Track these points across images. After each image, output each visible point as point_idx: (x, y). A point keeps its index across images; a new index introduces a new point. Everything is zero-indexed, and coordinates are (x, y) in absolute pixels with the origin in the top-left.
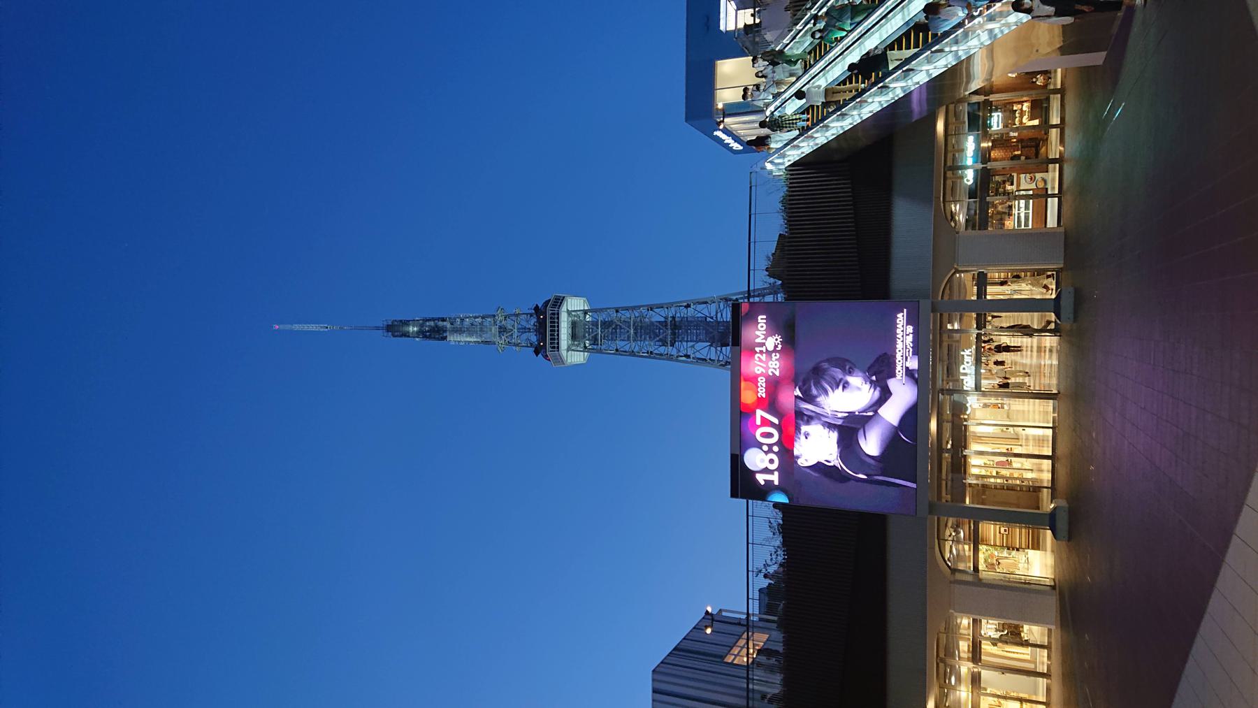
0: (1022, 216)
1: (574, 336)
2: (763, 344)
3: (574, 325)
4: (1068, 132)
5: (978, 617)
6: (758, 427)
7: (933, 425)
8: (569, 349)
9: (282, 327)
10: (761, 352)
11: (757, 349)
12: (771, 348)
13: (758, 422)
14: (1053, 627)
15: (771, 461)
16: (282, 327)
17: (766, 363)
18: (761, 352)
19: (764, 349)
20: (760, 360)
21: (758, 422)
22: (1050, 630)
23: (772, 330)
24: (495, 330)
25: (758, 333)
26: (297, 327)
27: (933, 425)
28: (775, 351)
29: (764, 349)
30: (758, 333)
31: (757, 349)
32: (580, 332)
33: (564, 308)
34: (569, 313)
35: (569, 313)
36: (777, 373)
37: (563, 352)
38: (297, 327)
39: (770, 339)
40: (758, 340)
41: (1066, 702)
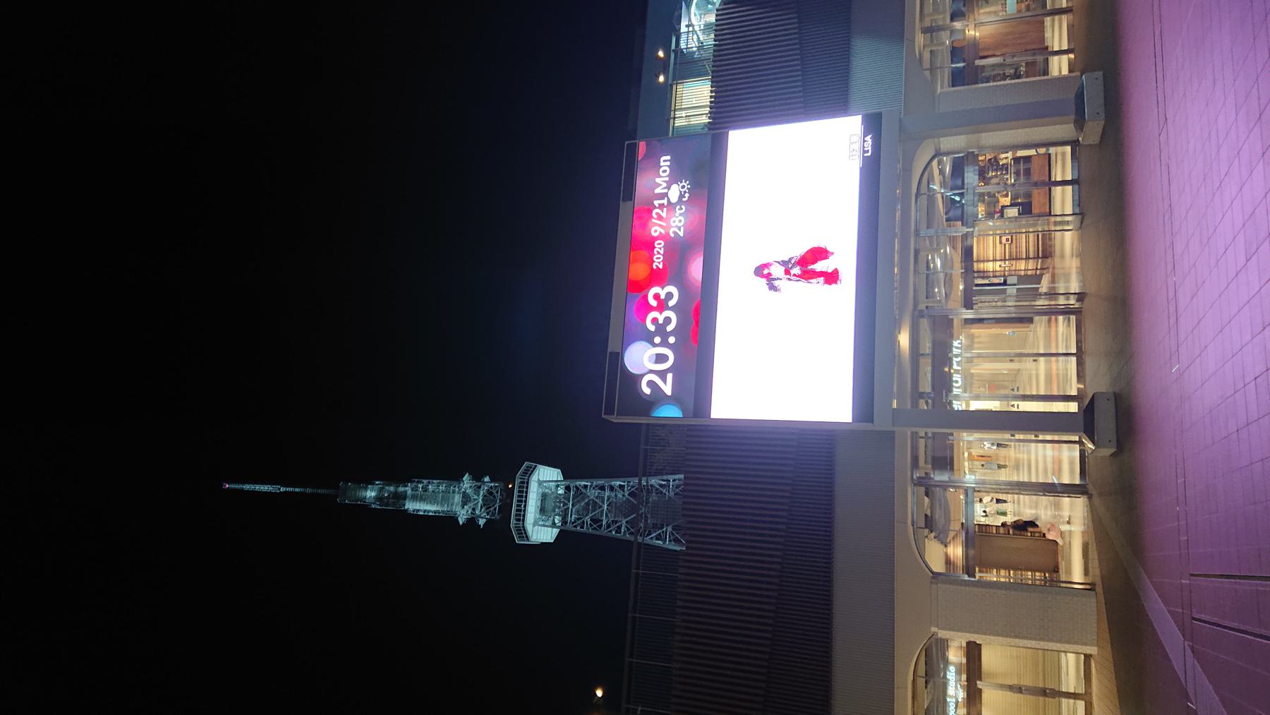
0: (1040, 459)
1: (542, 510)
2: (666, 195)
3: (544, 497)
4: (1089, 363)
6: (652, 309)
8: (535, 523)
9: (233, 486)
11: (656, 203)
12: (674, 199)
13: (670, 376)
15: (661, 358)
16: (233, 486)
17: (667, 220)
19: (665, 202)
20: (660, 217)
21: (670, 376)
24: (458, 498)
25: (658, 180)
26: (247, 487)
29: (665, 202)
30: (658, 180)
31: (656, 203)
32: (550, 504)
33: (534, 478)
34: (540, 483)
35: (540, 483)
36: (681, 234)
38: (247, 487)
40: (658, 191)
41: (1119, 713)
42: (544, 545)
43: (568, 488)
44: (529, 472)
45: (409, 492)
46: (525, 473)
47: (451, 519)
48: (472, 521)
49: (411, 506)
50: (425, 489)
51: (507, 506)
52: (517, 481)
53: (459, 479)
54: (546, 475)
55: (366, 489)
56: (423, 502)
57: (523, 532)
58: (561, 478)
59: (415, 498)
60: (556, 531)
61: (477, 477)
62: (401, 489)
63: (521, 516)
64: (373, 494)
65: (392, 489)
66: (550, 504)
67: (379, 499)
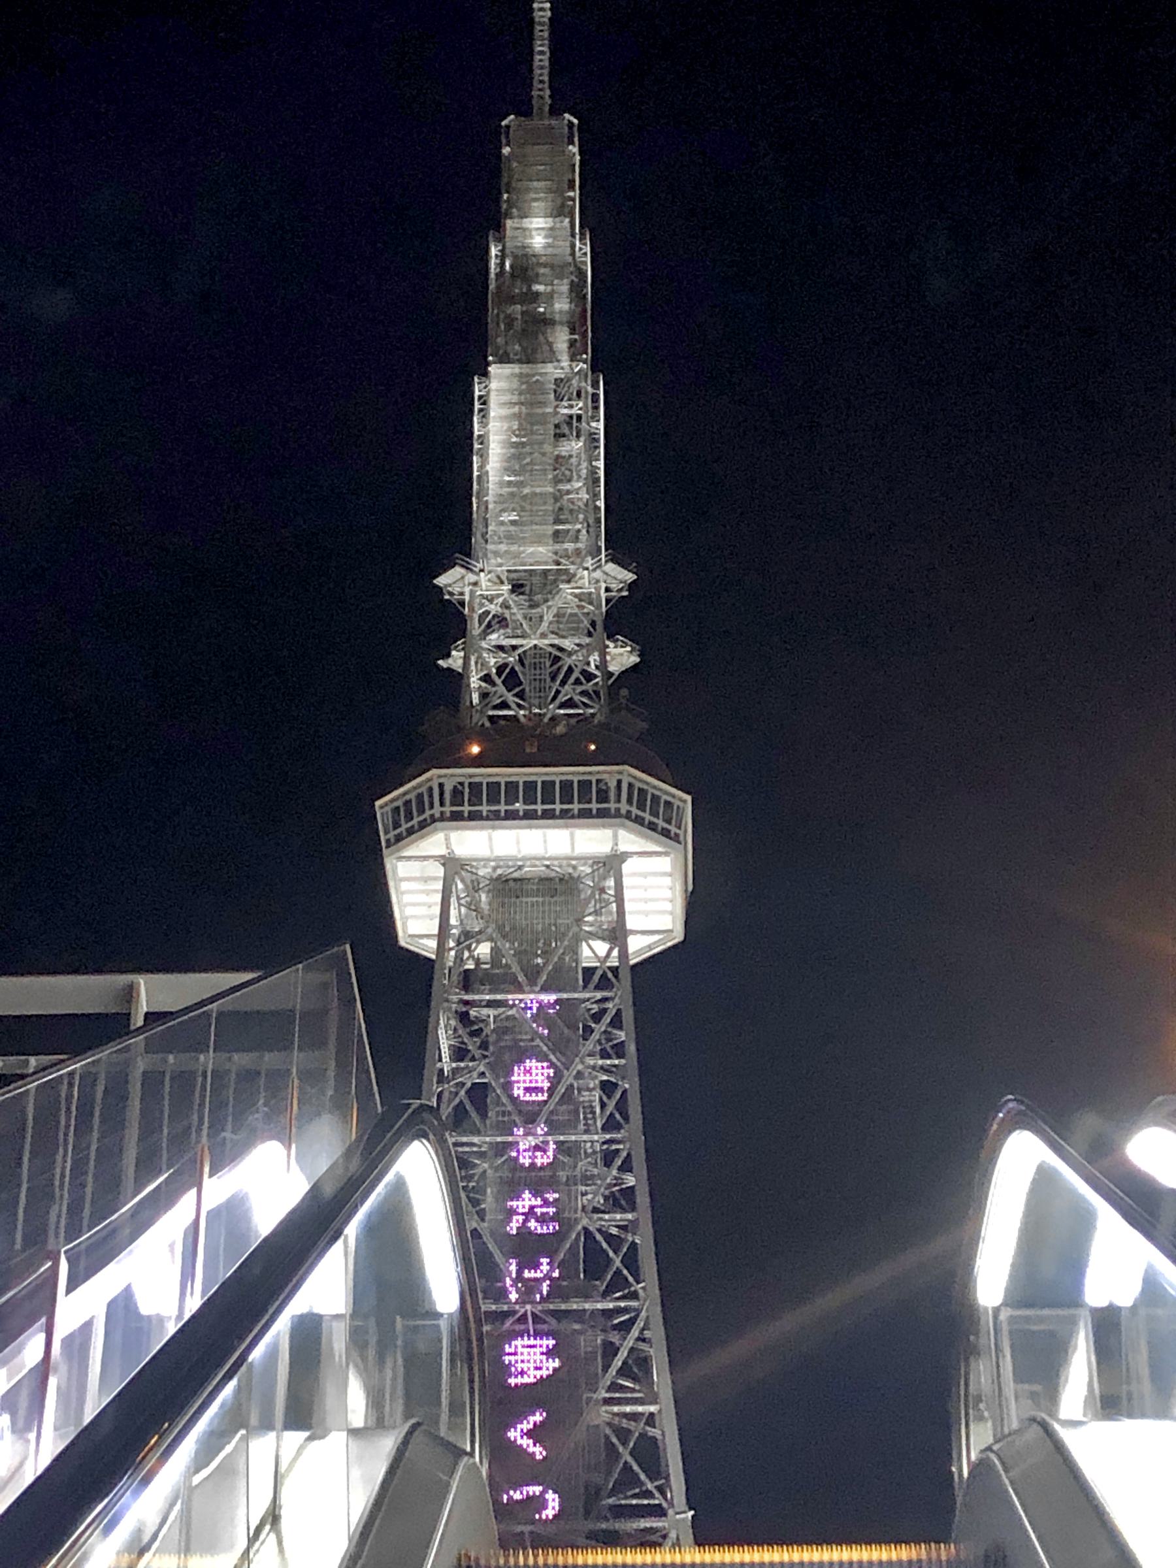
1: (510, 886)
3: (558, 886)
8: (453, 865)
24: (538, 555)
33: (629, 840)
34: (612, 864)
35: (612, 864)
37: (434, 843)
42: (696, 907)
43: (602, 978)
44: (651, 817)
45: (552, 371)
46: (641, 797)
47: (456, 538)
48: (450, 622)
49: (498, 388)
50: (566, 428)
51: (547, 752)
52: (608, 773)
53: (618, 549)
54: (653, 895)
55: (560, 211)
56: (529, 442)
57: (416, 820)
58: (639, 946)
59: (530, 394)
60: (428, 947)
61: (618, 619)
62: (561, 339)
63: (469, 806)
64: (538, 242)
65: (562, 305)
66: (532, 913)
67: (525, 268)
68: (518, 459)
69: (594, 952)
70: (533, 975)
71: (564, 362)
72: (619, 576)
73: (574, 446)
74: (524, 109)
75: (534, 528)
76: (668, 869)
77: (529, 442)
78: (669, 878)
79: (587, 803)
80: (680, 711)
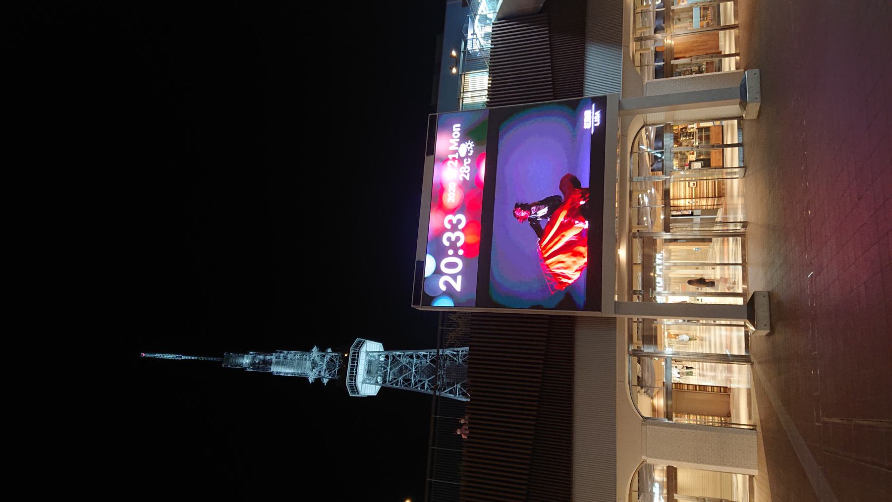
1: (369, 372)
2: (457, 151)
3: (370, 363)
4: (751, 270)
5: (674, 464)
7: (622, 253)
10: (454, 159)
12: (463, 154)
14: (755, 472)
18: (454, 159)
19: (456, 156)
21: (459, 278)
22: (751, 477)
23: (466, 136)
24: (308, 364)
25: (452, 141)
27: (622, 253)
28: (467, 156)
31: (450, 157)
32: (374, 368)
33: (363, 349)
34: (367, 353)
35: (367, 353)
37: (359, 385)
38: (158, 356)
39: (463, 145)
42: (370, 398)
44: (360, 345)
45: (274, 360)
46: (356, 346)
48: (318, 381)
49: (275, 369)
53: (309, 349)
54: (372, 347)
55: (243, 357)
56: (287, 365)
57: (354, 388)
58: (382, 349)
59: (278, 363)
60: (378, 388)
61: (322, 349)
62: (268, 357)
63: (353, 377)
64: (248, 361)
65: (262, 357)
66: (374, 368)
67: (253, 364)
68: (292, 366)
69: (382, 359)
70: (385, 368)
71: (273, 357)
72: (315, 349)
73: (289, 356)
74: (221, 363)
75: (305, 365)
76: (738, 349)
77: (287, 365)
78: (745, 367)
79: (356, 356)
80: (342, 342)
